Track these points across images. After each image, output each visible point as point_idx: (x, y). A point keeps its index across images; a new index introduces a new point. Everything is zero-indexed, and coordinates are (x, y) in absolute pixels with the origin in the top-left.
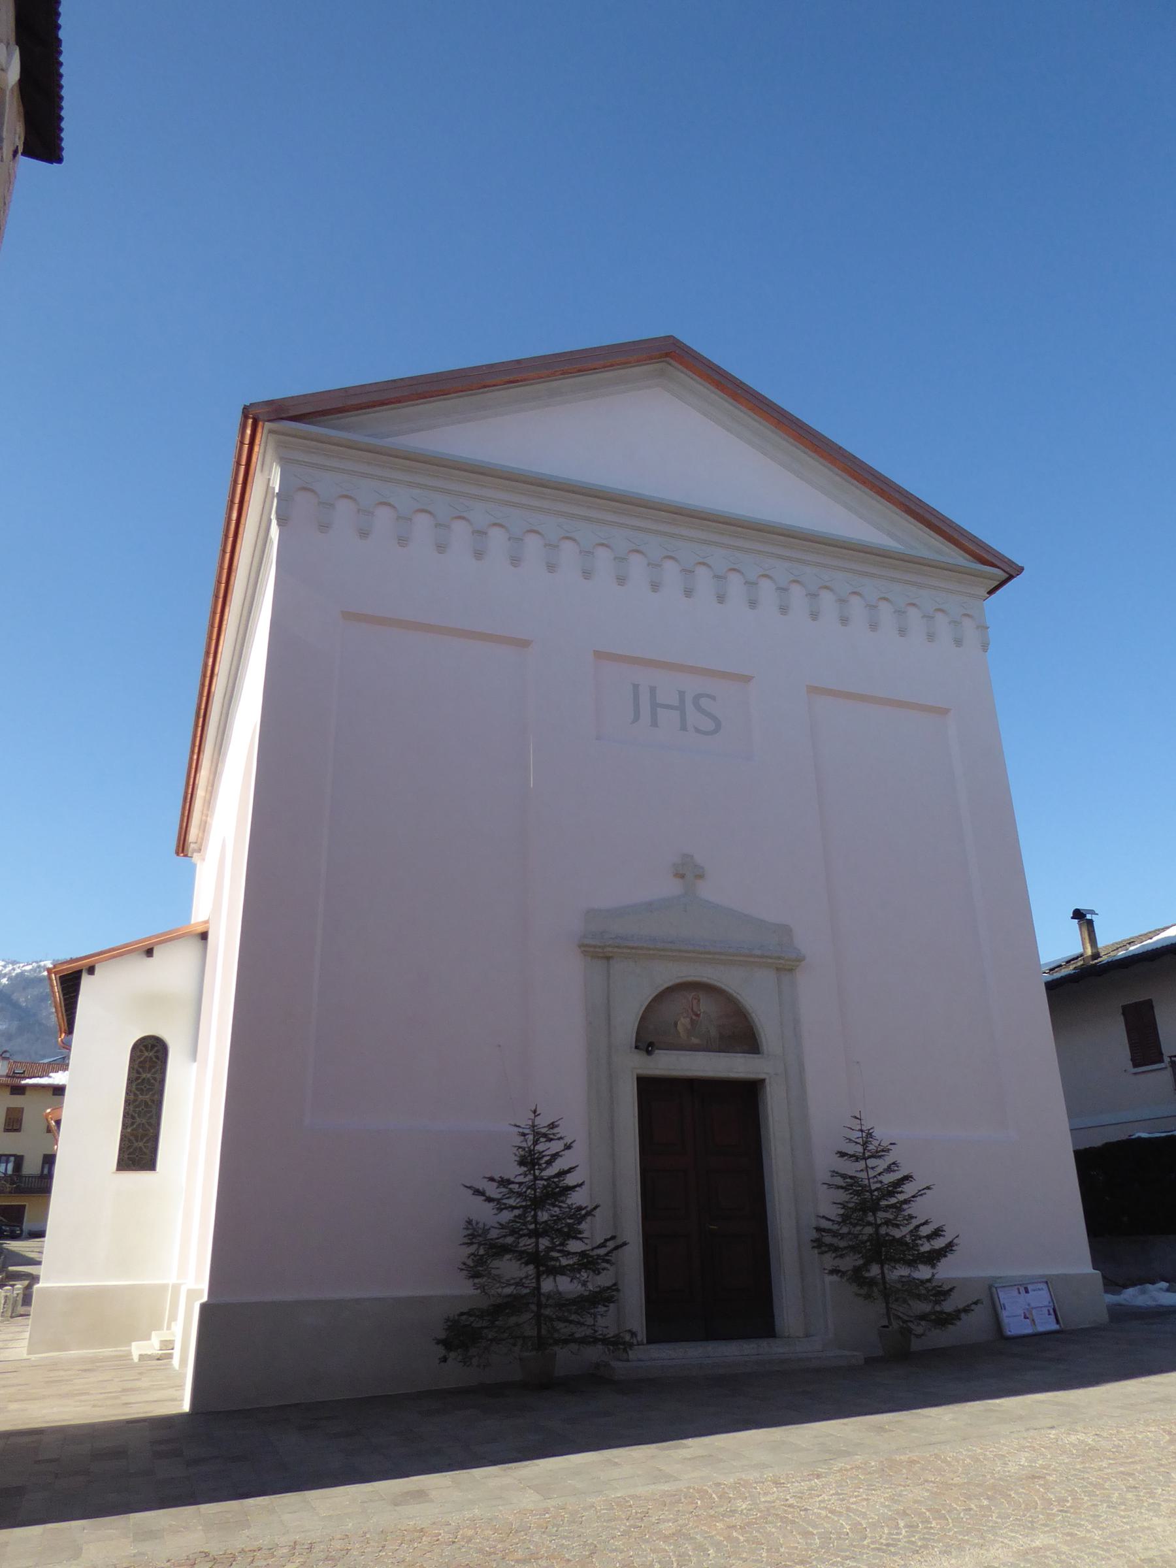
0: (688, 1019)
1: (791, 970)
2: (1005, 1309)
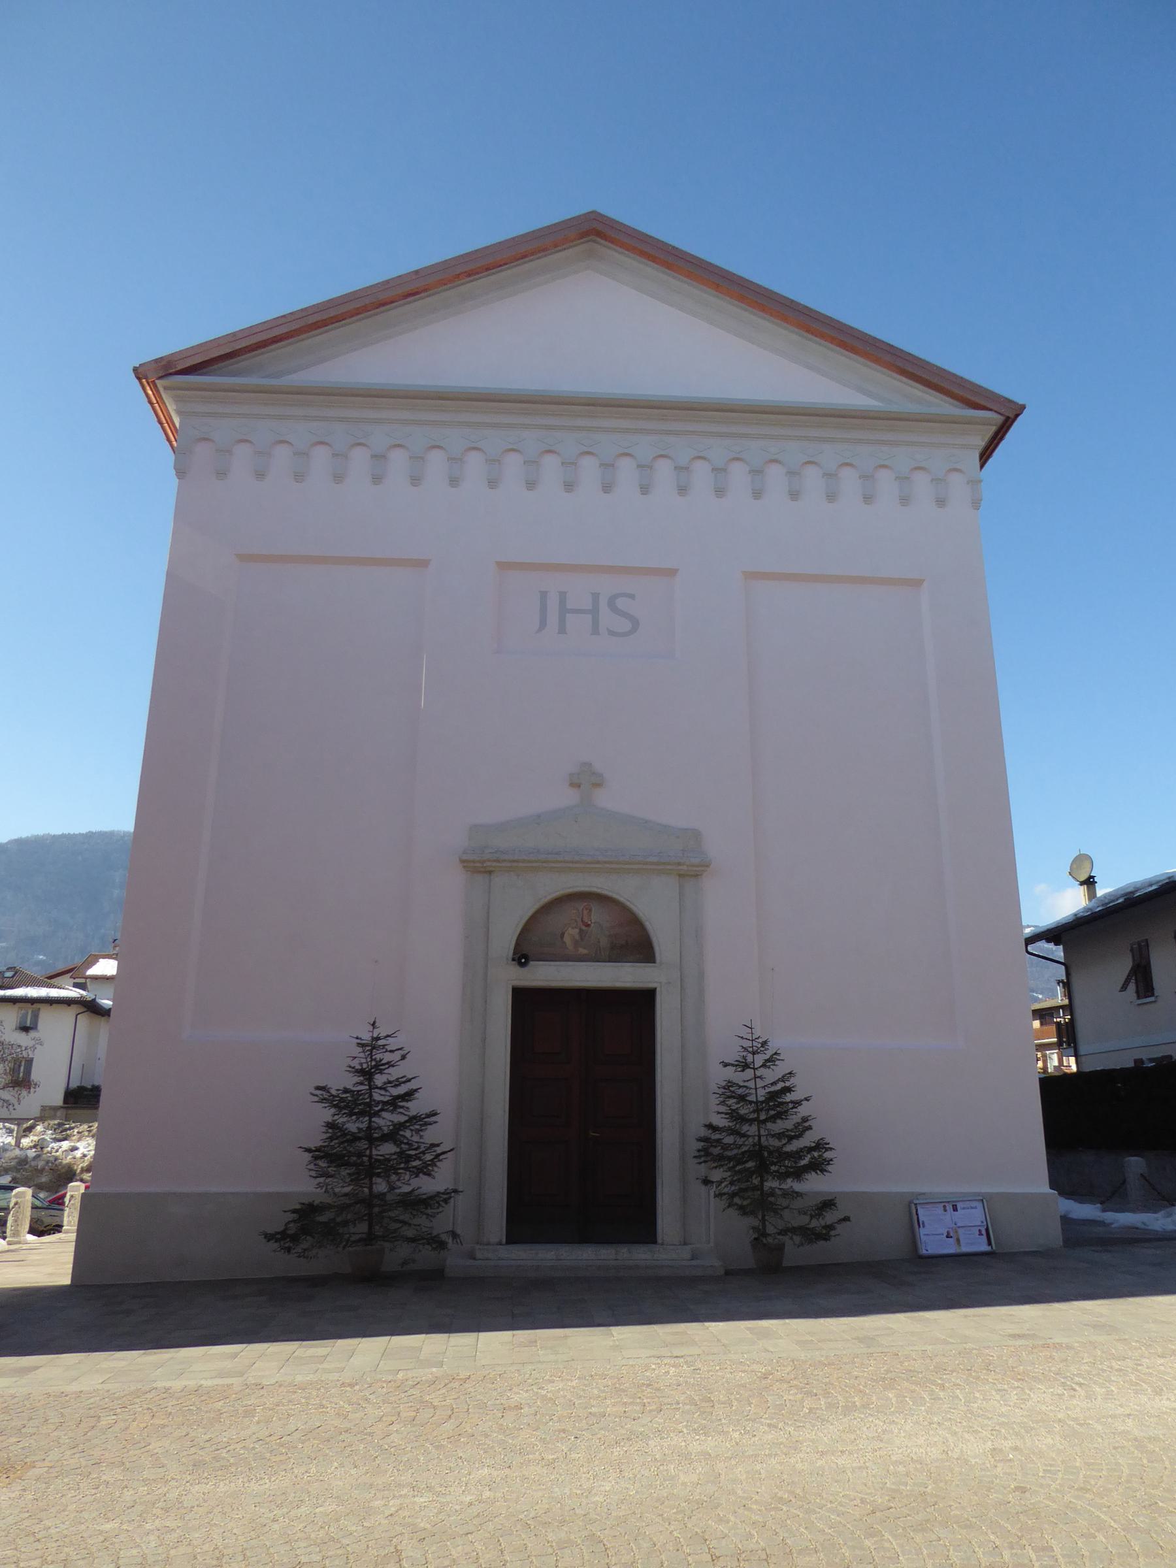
0: (577, 931)
1: (696, 876)
2: (924, 1227)
